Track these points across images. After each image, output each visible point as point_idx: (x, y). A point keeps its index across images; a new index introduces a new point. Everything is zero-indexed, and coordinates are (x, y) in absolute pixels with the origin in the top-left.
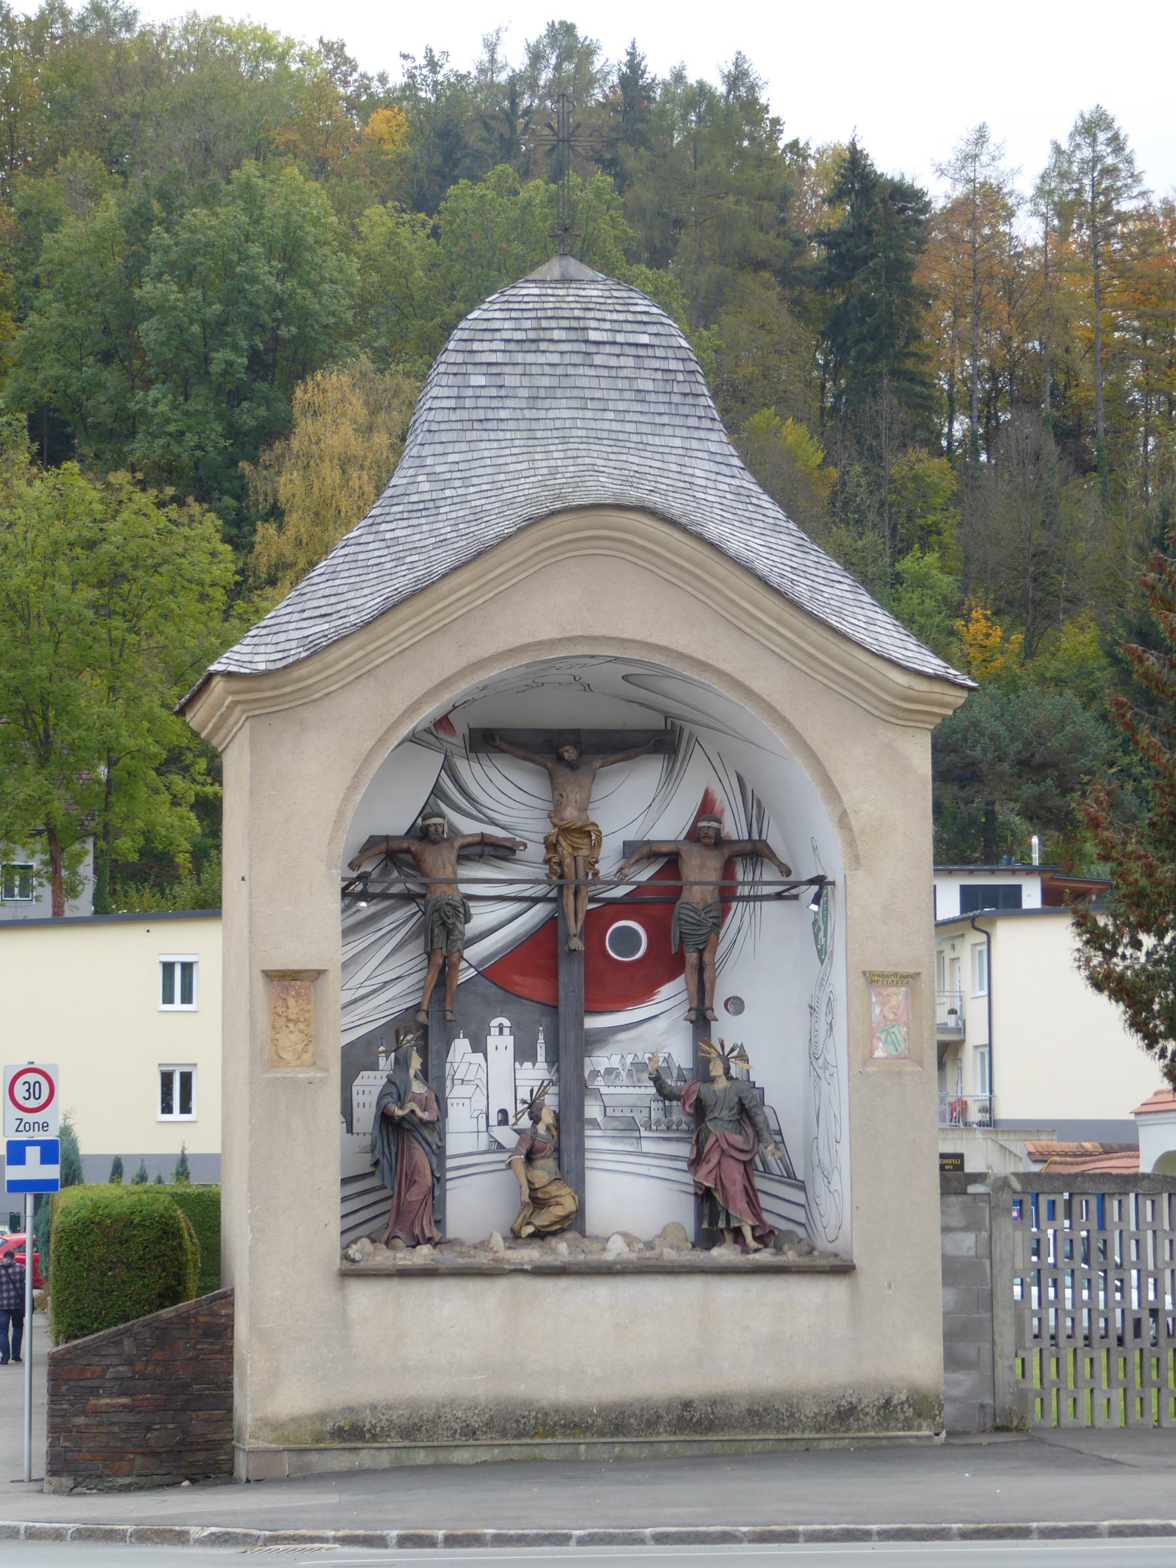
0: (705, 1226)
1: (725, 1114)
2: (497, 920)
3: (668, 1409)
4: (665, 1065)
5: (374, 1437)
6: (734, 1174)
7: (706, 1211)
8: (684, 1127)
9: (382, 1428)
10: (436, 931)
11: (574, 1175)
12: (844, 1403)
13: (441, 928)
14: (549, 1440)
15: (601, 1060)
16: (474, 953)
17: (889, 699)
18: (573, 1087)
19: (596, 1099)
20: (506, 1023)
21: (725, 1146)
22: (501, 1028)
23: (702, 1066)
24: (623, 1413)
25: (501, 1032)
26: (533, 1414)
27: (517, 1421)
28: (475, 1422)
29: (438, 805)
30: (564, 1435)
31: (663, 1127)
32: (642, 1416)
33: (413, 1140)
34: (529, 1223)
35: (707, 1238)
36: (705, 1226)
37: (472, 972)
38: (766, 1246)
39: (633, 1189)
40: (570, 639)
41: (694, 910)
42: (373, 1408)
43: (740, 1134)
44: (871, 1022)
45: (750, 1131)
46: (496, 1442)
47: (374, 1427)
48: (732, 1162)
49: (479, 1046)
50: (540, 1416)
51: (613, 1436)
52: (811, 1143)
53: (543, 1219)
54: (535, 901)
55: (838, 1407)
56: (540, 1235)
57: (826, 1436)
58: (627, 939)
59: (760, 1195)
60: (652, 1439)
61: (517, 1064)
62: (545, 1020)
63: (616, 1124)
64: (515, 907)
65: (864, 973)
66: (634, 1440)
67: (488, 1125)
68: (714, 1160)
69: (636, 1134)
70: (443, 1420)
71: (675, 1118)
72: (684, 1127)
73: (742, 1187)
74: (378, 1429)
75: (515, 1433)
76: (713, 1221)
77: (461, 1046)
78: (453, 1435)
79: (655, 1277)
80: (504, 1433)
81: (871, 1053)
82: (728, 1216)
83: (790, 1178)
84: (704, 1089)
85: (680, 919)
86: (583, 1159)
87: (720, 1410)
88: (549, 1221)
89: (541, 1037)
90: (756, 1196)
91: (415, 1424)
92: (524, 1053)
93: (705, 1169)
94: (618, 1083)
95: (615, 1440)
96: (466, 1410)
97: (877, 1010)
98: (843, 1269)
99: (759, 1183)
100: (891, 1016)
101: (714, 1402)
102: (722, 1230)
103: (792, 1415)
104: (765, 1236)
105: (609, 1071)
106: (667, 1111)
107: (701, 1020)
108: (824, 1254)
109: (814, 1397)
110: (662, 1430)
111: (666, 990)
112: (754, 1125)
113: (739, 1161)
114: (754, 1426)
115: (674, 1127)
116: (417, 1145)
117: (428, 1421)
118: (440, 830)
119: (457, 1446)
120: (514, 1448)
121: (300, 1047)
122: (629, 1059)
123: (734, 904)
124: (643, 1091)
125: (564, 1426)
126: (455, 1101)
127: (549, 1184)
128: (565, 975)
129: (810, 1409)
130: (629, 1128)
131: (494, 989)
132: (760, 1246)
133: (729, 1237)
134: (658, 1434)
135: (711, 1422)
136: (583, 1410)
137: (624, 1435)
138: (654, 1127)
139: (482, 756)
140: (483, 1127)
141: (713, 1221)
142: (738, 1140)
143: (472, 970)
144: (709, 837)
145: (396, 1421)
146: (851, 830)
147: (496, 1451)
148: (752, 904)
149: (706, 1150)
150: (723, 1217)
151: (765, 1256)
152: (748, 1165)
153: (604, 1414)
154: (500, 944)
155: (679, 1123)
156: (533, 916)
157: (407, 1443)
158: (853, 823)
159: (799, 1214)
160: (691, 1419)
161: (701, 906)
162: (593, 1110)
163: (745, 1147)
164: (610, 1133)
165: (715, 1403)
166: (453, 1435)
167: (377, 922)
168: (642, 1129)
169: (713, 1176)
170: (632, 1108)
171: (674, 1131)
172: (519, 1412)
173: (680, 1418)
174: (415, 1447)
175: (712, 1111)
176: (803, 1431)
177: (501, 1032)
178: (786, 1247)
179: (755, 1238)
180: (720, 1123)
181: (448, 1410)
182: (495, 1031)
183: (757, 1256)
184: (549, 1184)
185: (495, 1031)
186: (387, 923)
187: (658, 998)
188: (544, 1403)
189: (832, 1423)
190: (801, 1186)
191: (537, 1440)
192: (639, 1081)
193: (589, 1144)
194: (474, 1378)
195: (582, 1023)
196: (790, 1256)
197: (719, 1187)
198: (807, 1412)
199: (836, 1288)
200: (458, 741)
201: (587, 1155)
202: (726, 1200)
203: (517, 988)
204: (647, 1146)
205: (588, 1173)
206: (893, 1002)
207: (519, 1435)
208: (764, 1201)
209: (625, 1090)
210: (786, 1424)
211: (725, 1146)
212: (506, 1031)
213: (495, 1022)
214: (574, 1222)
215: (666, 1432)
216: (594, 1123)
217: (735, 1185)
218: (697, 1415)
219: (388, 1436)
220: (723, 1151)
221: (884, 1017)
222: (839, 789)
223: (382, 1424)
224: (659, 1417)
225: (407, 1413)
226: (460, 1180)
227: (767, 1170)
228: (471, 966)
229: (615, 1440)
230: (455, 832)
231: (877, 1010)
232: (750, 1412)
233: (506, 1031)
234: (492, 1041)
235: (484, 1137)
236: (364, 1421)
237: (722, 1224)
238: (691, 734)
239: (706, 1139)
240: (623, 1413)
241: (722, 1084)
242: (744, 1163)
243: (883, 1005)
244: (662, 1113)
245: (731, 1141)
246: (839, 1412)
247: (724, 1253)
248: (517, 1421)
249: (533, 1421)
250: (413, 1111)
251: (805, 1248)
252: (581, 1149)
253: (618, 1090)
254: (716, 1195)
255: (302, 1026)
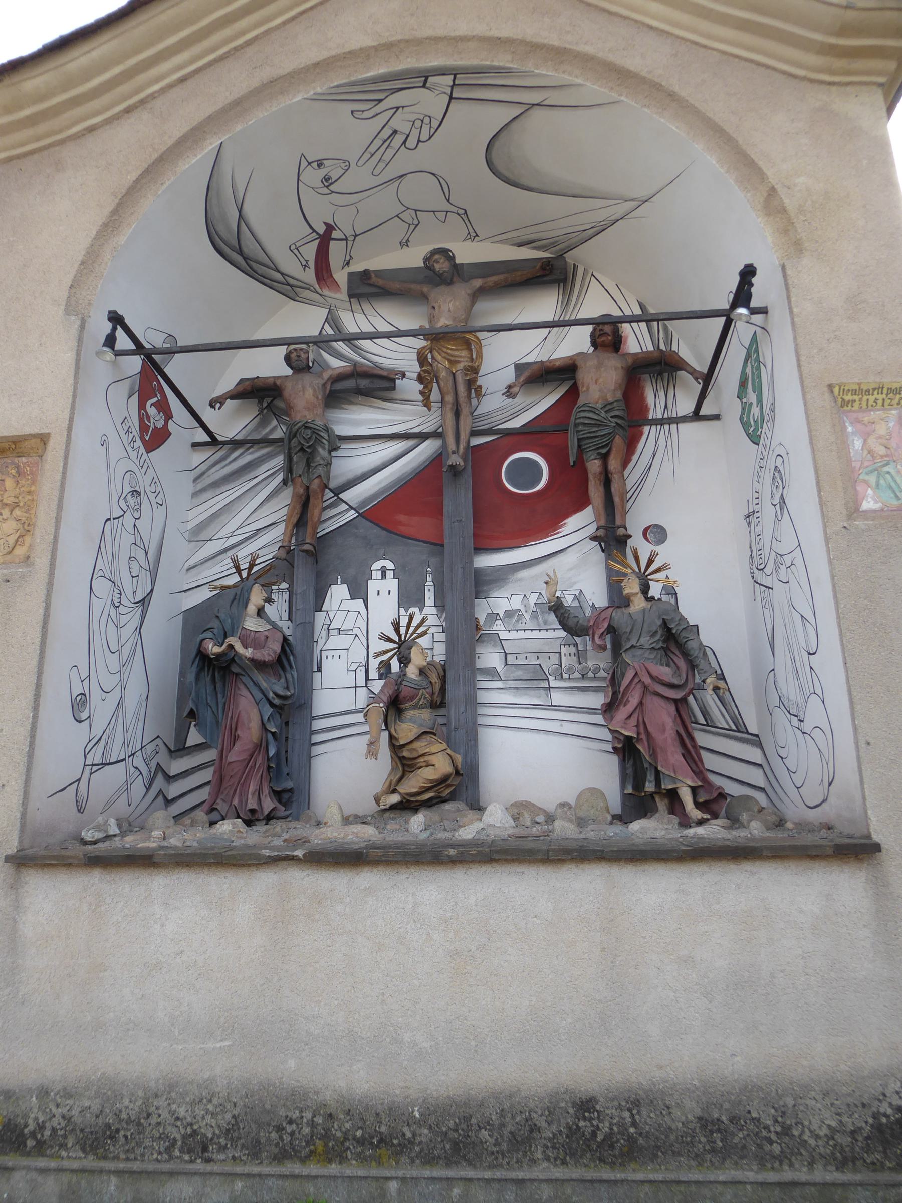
0: (629, 790)
1: (645, 641)
2: (376, 450)
3: (550, 1112)
4: (576, 603)
5: (41, 1148)
6: (662, 718)
7: (630, 771)
8: (602, 674)
9: (54, 1130)
10: (295, 458)
11: (465, 739)
12: (885, 1108)
13: (305, 455)
14: (334, 1169)
15: (502, 601)
16: (353, 495)
17: (818, 37)
18: (466, 634)
19: (494, 645)
20: (390, 565)
21: (647, 680)
22: (384, 571)
23: (618, 598)
24: (467, 1119)
25: (384, 576)
26: (308, 1115)
27: (280, 1129)
28: (208, 1127)
29: (321, 355)
30: (363, 1159)
31: (577, 675)
32: (503, 1125)
33: (242, 686)
34: (394, 791)
35: (638, 805)
36: (629, 790)
37: (352, 514)
38: (715, 816)
39: (541, 750)
40: (389, 46)
41: (593, 410)
42: (43, 1092)
43: (668, 665)
44: (849, 461)
45: (681, 663)
46: (239, 1169)
47: (41, 1127)
48: (658, 701)
49: (358, 591)
50: (319, 1120)
51: (449, 1164)
52: (765, 680)
53: (412, 785)
54: (422, 437)
55: (876, 1116)
56: (408, 806)
57: (858, 1177)
58: (529, 471)
59: (704, 755)
60: (520, 1175)
61: (402, 610)
62: (433, 561)
63: (519, 673)
64: (398, 446)
65: (831, 387)
66: (487, 1175)
67: (367, 679)
68: (634, 701)
69: (544, 684)
70: (154, 1120)
71: (590, 664)
72: (602, 674)
73: (674, 735)
74: (47, 1133)
75: (276, 1151)
76: (639, 785)
77: (338, 592)
78: (169, 1150)
79: (521, 868)
80: (255, 1151)
81: (857, 504)
82: (657, 773)
83: (739, 730)
84: (619, 616)
85: (576, 425)
86: (475, 715)
87: (648, 1118)
88: (434, 796)
89: (429, 579)
90: (699, 756)
91: (108, 1126)
92: (409, 597)
93: (622, 713)
94: (520, 626)
95: (451, 1173)
96: (193, 1103)
97: (858, 443)
98: (857, 850)
99: (702, 739)
100: (882, 451)
101: (634, 1102)
102: (652, 795)
103: (786, 1131)
104: (713, 803)
105: (509, 613)
106: (580, 656)
107: (612, 540)
108: (803, 826)
109: (826, 1094)
110: (539, 1155)
111: (574, 522)
112: (686, 654)
113: (668, 699)
114: (713, 1151)
115: (591, 675)
116: (244, 692)
117: (129, 1121)
118: (303, 356)
119: (172, 1174)
120: (270, 1182)
121: (11, 540)
122: (533, 599)
123: (646, 429)
124: (551, 634)
125: (360, 1142)
126: (330, 653)
127: (418, 738)
128: (459, 510)
129: (820, 1120)
130: (536, 678)
131: (376, 530)
132: (706, 816)
133: (662, 804)
134: (534, 1162)
135: (631, 1140)
136: (397, 1112)
137: (470, 1163)
138: (565, 676)
139: (367, 307)
140: (361, 681)
141: (639, 785)
142: (665, 672)
143: (353, 512)
144: (606, 334)
145: (77, 1119)
146: (784, 210)
147: (239, 1185)
148: (667, 427)
149: (622, 689)
150: (651, 777)
151: (713, 831)
152: (680, 704)
153: (432, 1120)
154: (383, 485)
155: (597, 670)
156: (420, 454)
157: (90, 1162)
158: (787, 201)
159: (756, 777)
160: (594, 1134)
161: (599, 406)
162: (490, 658)
163: (675, 681)
164: (512, 684)
165: (637, 1103)
166: (169, 1150)
167: (250, 472)
168: (551, 678)
169: (633, 721)
170: (538, 654)
171: (591, 679)
172: (282, 1112)
173: (573, 1132)
174: (101, 1171)
175: (628, 639)
176: (811, 1164)
177: (384, 576)
178: (744, 817)
179: (697, 805)
180: (640, 652)
181: (162, 1102)
182: (377, 575)
183: (700, 830)
184: (418, 738)
185: (377, 575)
186: (263, 470)
187: (565, 530)
188: (328, 1096)
189: (868, 1150)
190: (756, 741)
191: (313, 1169)
192: (545, 623)
193: (483, 697)
194: (210, 1045)
195: (471, 562)
196: (755, 830)
197: (643, 736)
198: (815, 1127)
199: (846, 885)
200: (343, 295)
201: (482, 710)
202: (654, 754)
203: (402, 528)
204: (558, 698)
205: (481, 730)
206: (881, 429)
207: (282, 1156)
208: (710, 761)
209: (528, 634)
210: (776, 1149)
211: (647, 680)
212: (390, 574)
213: (377, 565)
214: (460, 787)
215: (547, 1159)
216: (491, 673)
217: (664, 731)
218: (605, 1127)
219: (63, 1146)
220: (646, 687)
221: (870, 452)
222: (761, 164)
223: (55, 1123)
224: (534, 1128)
225: (96, 1106)
226: (334, 743)
227: (709, 723)
228: (351, 508)
229: (451, 1173)
230: (325, 366)
231: (858, 443)
232: (706, 1123)
233: (390, 574)
234: (373, 586)
235: (363, 693)
236: (25, 1116)
237: (650, 787)
238: (585, 271)
239: (623, 675)
240: (467, 1119)
241: (638, 603)
242: (676, 701)
243: (866, 437)
244: (575, 659)
245: (655, 674)
246: (878, 1128)
247: (653, 828)
248: (280, 1129)
249: (306, 1130)
250: (231, 647)
251: (772, 818)
252: (472, 703)
253: (521, 635)
254: (640, 747)
255: (17, 512)
